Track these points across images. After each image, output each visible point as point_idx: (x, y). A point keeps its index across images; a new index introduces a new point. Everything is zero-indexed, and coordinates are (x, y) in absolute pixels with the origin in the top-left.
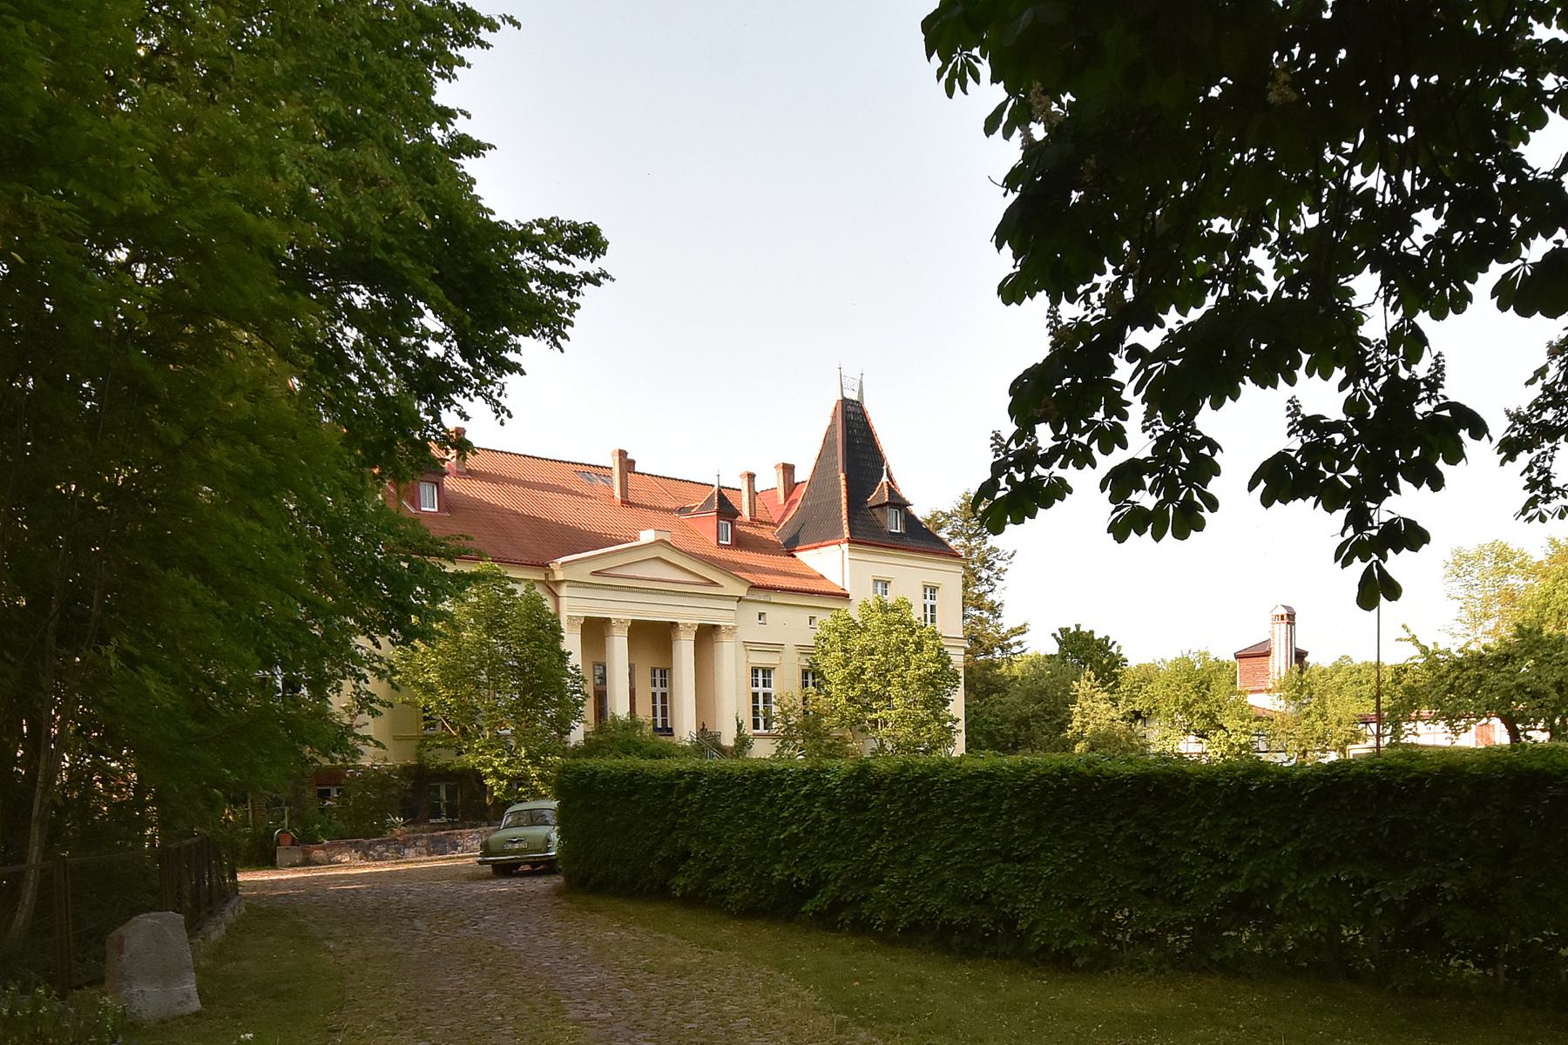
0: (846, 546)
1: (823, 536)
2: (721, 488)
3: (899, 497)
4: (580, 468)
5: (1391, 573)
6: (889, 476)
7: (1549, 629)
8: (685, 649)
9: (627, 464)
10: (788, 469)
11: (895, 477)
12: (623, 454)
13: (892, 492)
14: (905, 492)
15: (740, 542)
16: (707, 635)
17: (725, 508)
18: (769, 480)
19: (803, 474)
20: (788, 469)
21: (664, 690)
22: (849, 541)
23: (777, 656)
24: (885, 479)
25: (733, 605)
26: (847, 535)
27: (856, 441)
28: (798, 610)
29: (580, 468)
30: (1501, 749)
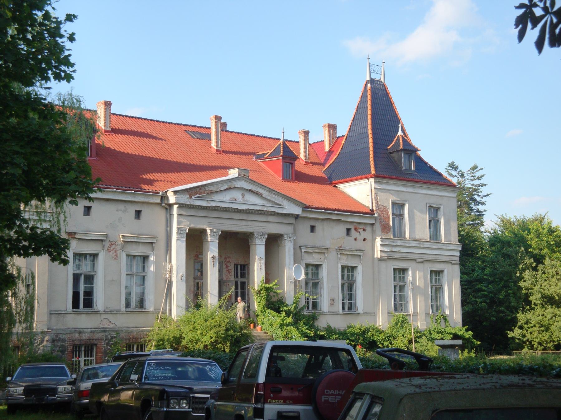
0: (372, 180)
1: (356, 173)
2: (285, 141)
3: (410, 145)
4: (188, 129)
5: (426, 159)
6: (403, 131)
7: (49, 203)
8: (259, 250)
9: (222, 126)
10: (332, 128)
11: (408, 131)
12: (218, 118)
13: (406, 142)
14: (415, 142)
15: (300, 177)
16: (273, 241)
17: (288, 154)
18: (320, 135)
19: (342, 131)
20: (332, 128)
21: (243, 280)
22: (375, 176)
23: (322, 257)
24: (400, 133)
25: (292, 221)
26: (373, 172)
27: (379, 106)
28: (201, 218)
29: (188, 129)
30: (353, 389)
